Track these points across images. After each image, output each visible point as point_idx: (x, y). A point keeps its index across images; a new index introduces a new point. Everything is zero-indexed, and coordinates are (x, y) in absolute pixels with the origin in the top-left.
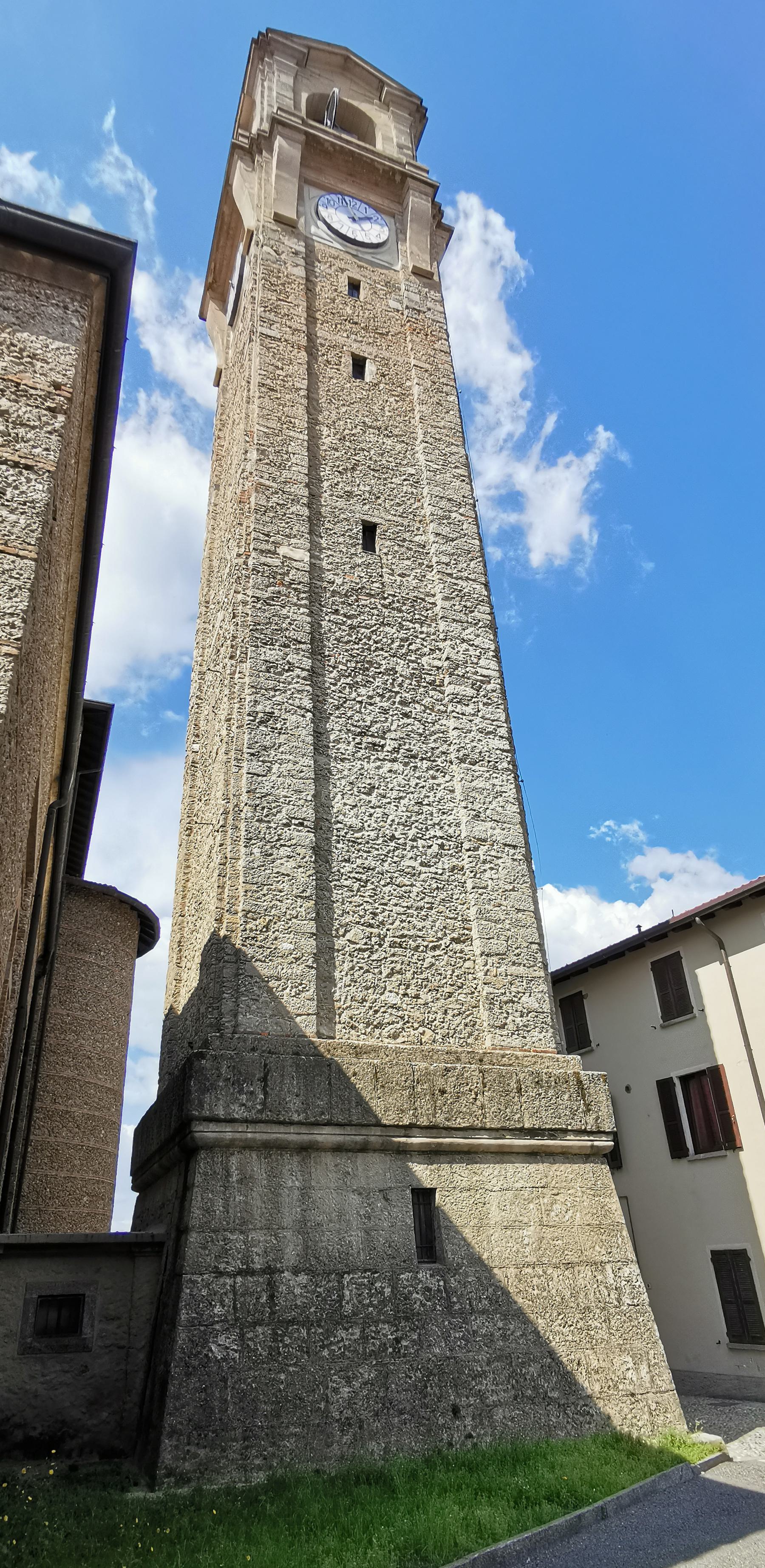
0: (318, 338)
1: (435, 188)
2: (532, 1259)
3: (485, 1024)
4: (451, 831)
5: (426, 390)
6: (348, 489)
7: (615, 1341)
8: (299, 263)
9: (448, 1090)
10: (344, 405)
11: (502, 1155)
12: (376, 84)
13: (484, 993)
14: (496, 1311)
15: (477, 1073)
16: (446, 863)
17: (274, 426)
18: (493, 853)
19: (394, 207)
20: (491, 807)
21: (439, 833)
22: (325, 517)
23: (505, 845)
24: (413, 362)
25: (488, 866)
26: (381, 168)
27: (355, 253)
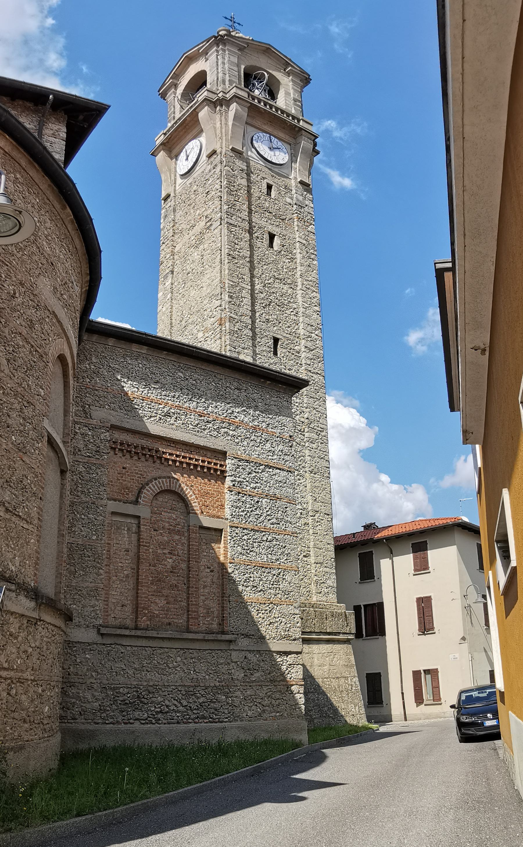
0: (253, 222)
1: (316, 137)
3: (314, 591)
4: (305, 506)
6: (267, 317)
8: (243, 176)
10: (265, 265)
11: (318, 641)
12: (285, 64)
13: (315, 579)
14: (315, 692)
16: (303, 521)
18: (321, 518)
19: (291, 140)
20: (321, 496)
21: (300, 507)
22: (257, 335)
23: (325, 514)
24: (297, 240)
25: (319, 523)
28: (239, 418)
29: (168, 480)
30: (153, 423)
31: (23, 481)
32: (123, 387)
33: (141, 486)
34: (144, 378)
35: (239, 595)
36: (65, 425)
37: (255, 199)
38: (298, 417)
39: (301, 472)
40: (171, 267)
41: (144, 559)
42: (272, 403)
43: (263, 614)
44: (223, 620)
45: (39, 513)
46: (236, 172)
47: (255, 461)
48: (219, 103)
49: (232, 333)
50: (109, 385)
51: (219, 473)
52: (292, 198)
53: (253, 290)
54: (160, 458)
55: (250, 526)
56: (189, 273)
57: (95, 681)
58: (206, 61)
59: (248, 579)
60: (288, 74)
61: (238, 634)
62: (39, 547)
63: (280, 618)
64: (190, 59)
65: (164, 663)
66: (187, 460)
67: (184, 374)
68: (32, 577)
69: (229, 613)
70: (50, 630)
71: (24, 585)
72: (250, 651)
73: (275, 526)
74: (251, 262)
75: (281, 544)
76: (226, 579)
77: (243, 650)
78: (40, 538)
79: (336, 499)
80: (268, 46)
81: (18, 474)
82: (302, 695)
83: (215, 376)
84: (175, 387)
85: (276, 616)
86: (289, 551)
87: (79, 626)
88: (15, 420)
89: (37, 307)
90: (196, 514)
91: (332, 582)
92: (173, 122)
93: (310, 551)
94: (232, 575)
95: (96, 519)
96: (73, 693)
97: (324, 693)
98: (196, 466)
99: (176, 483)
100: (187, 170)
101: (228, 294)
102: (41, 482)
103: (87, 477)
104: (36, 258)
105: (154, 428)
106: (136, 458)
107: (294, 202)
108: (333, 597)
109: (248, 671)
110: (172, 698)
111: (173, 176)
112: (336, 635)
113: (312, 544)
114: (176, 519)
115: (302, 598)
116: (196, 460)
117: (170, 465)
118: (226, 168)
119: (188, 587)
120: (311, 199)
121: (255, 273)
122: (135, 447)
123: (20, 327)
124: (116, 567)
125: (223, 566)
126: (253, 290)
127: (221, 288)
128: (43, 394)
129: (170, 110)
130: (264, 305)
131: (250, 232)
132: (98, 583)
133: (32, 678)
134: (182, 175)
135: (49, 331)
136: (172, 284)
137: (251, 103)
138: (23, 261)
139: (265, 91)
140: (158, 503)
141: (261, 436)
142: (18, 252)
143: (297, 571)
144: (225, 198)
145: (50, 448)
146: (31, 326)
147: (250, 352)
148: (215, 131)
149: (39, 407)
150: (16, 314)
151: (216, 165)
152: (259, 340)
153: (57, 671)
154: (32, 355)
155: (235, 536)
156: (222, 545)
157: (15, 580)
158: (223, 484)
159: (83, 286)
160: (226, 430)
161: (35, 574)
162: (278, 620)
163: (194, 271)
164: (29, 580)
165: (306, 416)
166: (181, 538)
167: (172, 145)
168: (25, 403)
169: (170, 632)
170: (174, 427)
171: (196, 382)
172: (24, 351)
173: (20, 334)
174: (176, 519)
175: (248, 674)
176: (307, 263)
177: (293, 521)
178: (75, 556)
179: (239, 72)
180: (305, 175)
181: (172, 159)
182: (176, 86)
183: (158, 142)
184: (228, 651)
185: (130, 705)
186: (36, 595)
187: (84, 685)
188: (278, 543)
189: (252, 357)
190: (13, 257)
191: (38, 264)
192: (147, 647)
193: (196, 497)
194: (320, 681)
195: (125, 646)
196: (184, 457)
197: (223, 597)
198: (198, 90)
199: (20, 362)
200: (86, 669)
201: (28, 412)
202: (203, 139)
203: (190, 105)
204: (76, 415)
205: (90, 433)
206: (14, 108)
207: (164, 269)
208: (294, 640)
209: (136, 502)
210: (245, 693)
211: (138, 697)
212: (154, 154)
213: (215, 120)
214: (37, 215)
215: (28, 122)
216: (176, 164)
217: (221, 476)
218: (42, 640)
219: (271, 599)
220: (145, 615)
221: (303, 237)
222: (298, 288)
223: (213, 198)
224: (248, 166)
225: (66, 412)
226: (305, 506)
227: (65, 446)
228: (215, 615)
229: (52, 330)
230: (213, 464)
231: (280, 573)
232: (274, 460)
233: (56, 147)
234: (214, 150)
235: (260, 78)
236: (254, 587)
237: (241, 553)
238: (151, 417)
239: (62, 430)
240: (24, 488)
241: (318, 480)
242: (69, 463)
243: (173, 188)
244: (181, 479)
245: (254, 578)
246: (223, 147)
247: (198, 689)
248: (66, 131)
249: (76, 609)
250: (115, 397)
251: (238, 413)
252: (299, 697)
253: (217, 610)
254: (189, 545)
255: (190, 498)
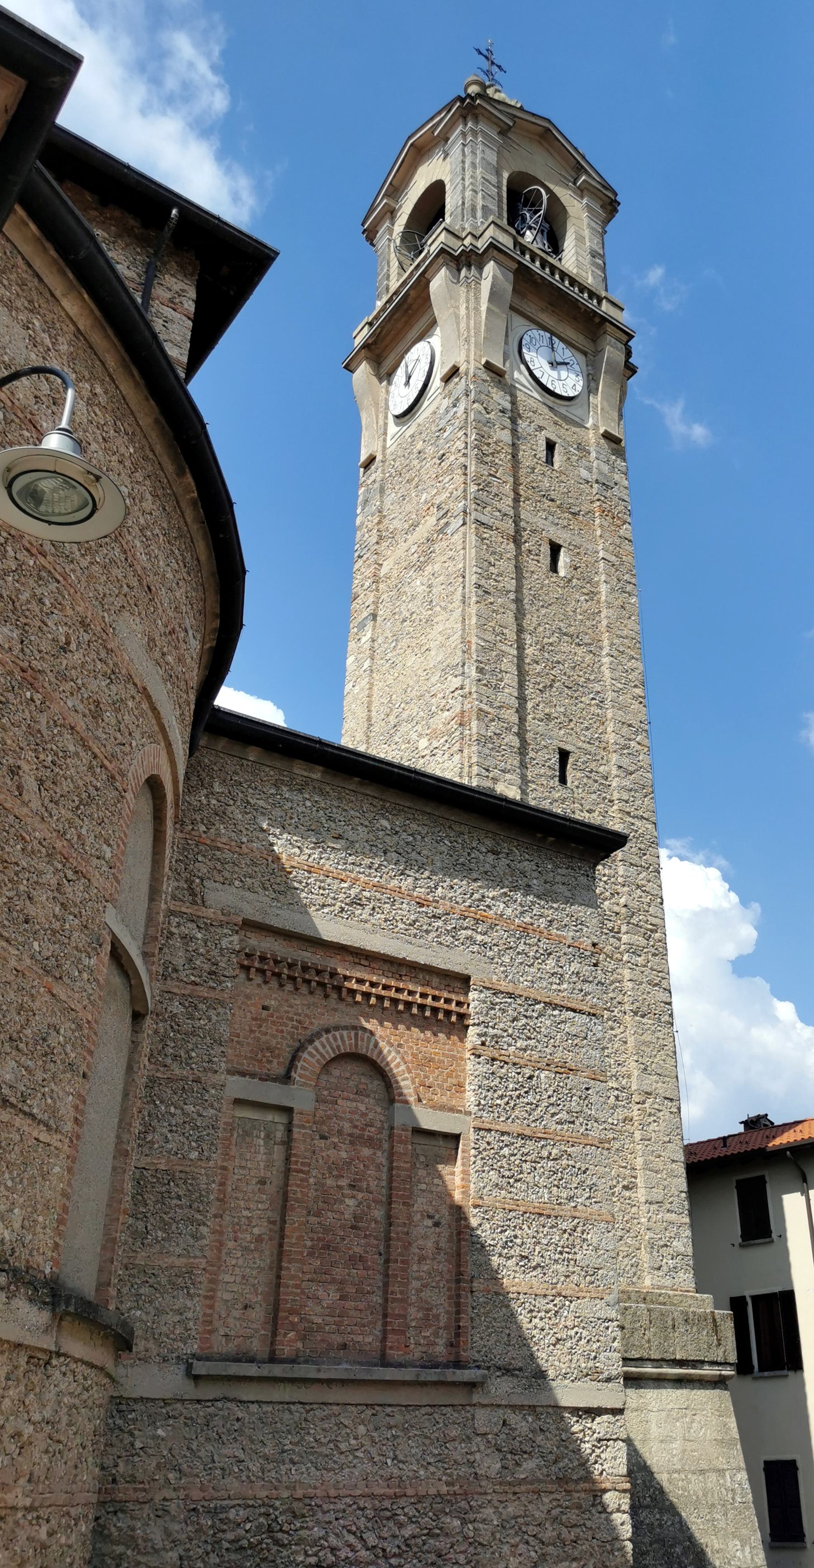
1: (631, 337)
2: (678, 1467)
3: (646, 1265)
4: (624, 1082)
5: (613, 590)
6: (547, 711)
7: (731, 1529)
8: (505, 424)
9: (626, 1326)
10: (543, 606)
11: (659, 1381)
14: (655, 1507)
15: (645, 1312)
16: (620, 1114)
17: (489, 638)
18: (656, 1106)
21: (615, 1085)
23: (666, 1098)
24: (601, 554)
25: (652, 1118)
26: (583, 308)
27: (551, 405)
28: (494, 908)
29: (353, 1033)
30: (329, 917)
31: (49, 1038)
32: (272, 845)
33: (297, 1044)
34: (313, 827)
35: (494, 1277)
36: (150, 919)
37: (525, 471)
38: (607, 903)
39: (615, 1013)
40: (372, 607)
41: (297, 1200)
42: (558, 878)
43: (541, 1319)
44: (458, 1335)
45: (76, 1108)
46: (492, 416)
47: (525, 994)
48: (464, 260)
49: (482, 740)
50: (245, 840)
51: (454, 1018)
52: (590, 470)
53: (521, 657)
54: (338, 989)
55: (515, 1128)
56: (404, 621)
57: (173, 1495)
58: (444, 159)
59: (511, 1241)
60: (581, 191)
61: (488, 1368)
62: (69, 1184)
63: (576, 1329)
64: (419, 152)
65: (330, 1441)
66: (393, 994)
67: (392, 823)
68: (49, 1254)
69: (472, 1318)
70: (80, 1377)
71: (27, 1272)
72: (513, 1407)
73: (566, 1127)
74: (518, 601)
75: (577, 1166)
76: (466, 1240)
77: (499, 1406)
78: (73, 1162)
79: (685, 1057)
80: (547, 125)
81: (39, 1023)
82: (626, 1517)
83: (450, 827)
84: (373, 847)
85: (569, 1323)
86: (595, 1180)
87: (145, 1360)
88: (43, 908)
89: (112, 677)
90: (406, 1102)
91: (683, 1244)
92: (385, 298)
93: (635, 1177)
94: (479, 1232)
95: (201, 1115)
96: (120, 1529)
97: (672, 1510)
98: (408, 1005)
99: (369, 1039)
100: (406, 407)
101: (476, 664)
102: (88, 1039)
103: (187, 1025)
104: (117, 572)
105: (330, 928)
106: (289, 987)
107: (594, 477)
108: (686, 1279)
109: (509, 1456)
110: (344, 1527)
111: (381, 416)
112: (694, 1367)
113: (639, 1161)
114: (366, 1115)
115: (621, 1279)
116: (411, 993)
117: (357, 1003)
118: (476, 405)
119: (387, 1261)
120: (624, 469)
121: (525, 623)
122: (290, 966)
123: (72, 713)
124: (236, 1220)
125: (458, 1213)
126: (521, 657)
127: (464, 652)
128: (108, 855)
129: (382, 269)
130: (540, 687)
131: (517, 540)
132: (195, 1257)
133: (28, 1502)
134: (397, 417)
135: (132, 727)
136: (373, 641)
137: (519, 263)
138: (90, 577)
139: (542, 232)
140: (332, 1080)
141: (537, 944)
142: (83, 555)
143: (611, 1221)
144: (472, 468)
145: (114, 967)
146: (96, 713)
147: (514, 777)
148: (458, 324)
149: (98, 880)
150: (68, 686)
151: (457, 400)
152: (532, 754)
153: (89, 1476)
154: (94, 774)
155: (485, 1150)
156: (458, 1167)
157: (7, 1261)
158: (462, 1040)
159: (207, 638)
160: (469, 932)
161: (56, 1245)
162: (572, 1333)
163: (414, 616)
164: (40, 1259)
165: (622, 901)
166: (374, 1154)
167: (381, 352)
168: (70, 874)
169: (345, 1366)
170: (368, 926)
171: (415, 839)
172: (77, 766)
173: (72, 728)
174: (366, 1115)
175: (511, 1464)
176: (619, 602)
177: (601, 1116)
178: (151, 1197)
179: (500, 182)
180: (613, 420)
181: (381, 380)
182: (391, 213)
183: (358, 341)
184: (468, 1408)
185: (249, 1552)
186: (53, 1296)
187: (147, 1506)
188: (571, 1163)
189: (520, 788)
190: (72, 566)
191: (122, 586)
192: (294, 1403)
193: (408, 1067)
194: (663, 1478)
195: (245, 1402)
196: (386, 987)
197: (458, 1281)
198: (429, 228)
199: (66, 786)
200: (154, 1464)
201: (75, 892)
202: (436, 340)
203: (416, 263)
204: (174, 897)
205: (199, 936)
206: (104, 222)
207: (360, 610)
208: (608, 1380)
209: (286, 1078)
210: (504, 1512)
211: (270, 1530)
212: (350, 367)
213: (457, 300)
214: (127, 481)
215: (125, 263)
216: (388, 392)
217: (457, 1024)
218: (59, 1403)
219: (559, 1286)
220: (293, 1326)
221: (611, 548)
222: (604, 653)
223: (450, 470)
224: (513, 403)
225: (154, 893)
226: (624, 1082)
227: (146, 962)
228: (442, 1324)
229: (138, 726)
230: (442, 1001)
231: (576, 1227)
232: (564, 992)
233: (174, 333)
234: (454, 366)
235: (533, 201)
236: (523, 1257)
237: (497, 1185)
238: (324, 906)
239: (142, 930)
240: (49, 1053)
241: (649, 1029)
242: (153, 997)
243: (380, 443)
244: (379, 1031)
245: (522, 1238)
246: (469, 360)
247: (402, 1502)
248: (194, 296)
249: (141, 1320)
250: (254, 864)
251: (493, 899)
252: (619, 1521)
253: (447, 1312)
254: (391, 1169)
255: (395, 1071)
